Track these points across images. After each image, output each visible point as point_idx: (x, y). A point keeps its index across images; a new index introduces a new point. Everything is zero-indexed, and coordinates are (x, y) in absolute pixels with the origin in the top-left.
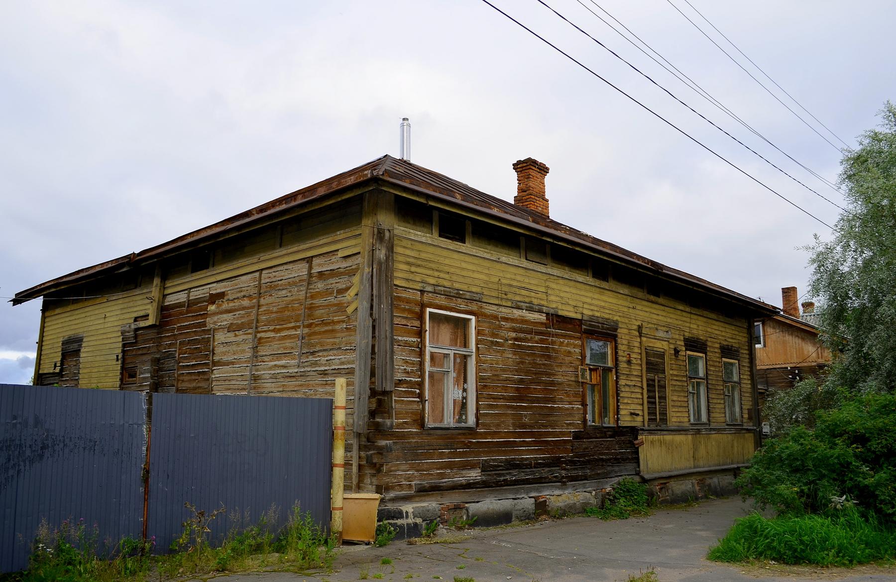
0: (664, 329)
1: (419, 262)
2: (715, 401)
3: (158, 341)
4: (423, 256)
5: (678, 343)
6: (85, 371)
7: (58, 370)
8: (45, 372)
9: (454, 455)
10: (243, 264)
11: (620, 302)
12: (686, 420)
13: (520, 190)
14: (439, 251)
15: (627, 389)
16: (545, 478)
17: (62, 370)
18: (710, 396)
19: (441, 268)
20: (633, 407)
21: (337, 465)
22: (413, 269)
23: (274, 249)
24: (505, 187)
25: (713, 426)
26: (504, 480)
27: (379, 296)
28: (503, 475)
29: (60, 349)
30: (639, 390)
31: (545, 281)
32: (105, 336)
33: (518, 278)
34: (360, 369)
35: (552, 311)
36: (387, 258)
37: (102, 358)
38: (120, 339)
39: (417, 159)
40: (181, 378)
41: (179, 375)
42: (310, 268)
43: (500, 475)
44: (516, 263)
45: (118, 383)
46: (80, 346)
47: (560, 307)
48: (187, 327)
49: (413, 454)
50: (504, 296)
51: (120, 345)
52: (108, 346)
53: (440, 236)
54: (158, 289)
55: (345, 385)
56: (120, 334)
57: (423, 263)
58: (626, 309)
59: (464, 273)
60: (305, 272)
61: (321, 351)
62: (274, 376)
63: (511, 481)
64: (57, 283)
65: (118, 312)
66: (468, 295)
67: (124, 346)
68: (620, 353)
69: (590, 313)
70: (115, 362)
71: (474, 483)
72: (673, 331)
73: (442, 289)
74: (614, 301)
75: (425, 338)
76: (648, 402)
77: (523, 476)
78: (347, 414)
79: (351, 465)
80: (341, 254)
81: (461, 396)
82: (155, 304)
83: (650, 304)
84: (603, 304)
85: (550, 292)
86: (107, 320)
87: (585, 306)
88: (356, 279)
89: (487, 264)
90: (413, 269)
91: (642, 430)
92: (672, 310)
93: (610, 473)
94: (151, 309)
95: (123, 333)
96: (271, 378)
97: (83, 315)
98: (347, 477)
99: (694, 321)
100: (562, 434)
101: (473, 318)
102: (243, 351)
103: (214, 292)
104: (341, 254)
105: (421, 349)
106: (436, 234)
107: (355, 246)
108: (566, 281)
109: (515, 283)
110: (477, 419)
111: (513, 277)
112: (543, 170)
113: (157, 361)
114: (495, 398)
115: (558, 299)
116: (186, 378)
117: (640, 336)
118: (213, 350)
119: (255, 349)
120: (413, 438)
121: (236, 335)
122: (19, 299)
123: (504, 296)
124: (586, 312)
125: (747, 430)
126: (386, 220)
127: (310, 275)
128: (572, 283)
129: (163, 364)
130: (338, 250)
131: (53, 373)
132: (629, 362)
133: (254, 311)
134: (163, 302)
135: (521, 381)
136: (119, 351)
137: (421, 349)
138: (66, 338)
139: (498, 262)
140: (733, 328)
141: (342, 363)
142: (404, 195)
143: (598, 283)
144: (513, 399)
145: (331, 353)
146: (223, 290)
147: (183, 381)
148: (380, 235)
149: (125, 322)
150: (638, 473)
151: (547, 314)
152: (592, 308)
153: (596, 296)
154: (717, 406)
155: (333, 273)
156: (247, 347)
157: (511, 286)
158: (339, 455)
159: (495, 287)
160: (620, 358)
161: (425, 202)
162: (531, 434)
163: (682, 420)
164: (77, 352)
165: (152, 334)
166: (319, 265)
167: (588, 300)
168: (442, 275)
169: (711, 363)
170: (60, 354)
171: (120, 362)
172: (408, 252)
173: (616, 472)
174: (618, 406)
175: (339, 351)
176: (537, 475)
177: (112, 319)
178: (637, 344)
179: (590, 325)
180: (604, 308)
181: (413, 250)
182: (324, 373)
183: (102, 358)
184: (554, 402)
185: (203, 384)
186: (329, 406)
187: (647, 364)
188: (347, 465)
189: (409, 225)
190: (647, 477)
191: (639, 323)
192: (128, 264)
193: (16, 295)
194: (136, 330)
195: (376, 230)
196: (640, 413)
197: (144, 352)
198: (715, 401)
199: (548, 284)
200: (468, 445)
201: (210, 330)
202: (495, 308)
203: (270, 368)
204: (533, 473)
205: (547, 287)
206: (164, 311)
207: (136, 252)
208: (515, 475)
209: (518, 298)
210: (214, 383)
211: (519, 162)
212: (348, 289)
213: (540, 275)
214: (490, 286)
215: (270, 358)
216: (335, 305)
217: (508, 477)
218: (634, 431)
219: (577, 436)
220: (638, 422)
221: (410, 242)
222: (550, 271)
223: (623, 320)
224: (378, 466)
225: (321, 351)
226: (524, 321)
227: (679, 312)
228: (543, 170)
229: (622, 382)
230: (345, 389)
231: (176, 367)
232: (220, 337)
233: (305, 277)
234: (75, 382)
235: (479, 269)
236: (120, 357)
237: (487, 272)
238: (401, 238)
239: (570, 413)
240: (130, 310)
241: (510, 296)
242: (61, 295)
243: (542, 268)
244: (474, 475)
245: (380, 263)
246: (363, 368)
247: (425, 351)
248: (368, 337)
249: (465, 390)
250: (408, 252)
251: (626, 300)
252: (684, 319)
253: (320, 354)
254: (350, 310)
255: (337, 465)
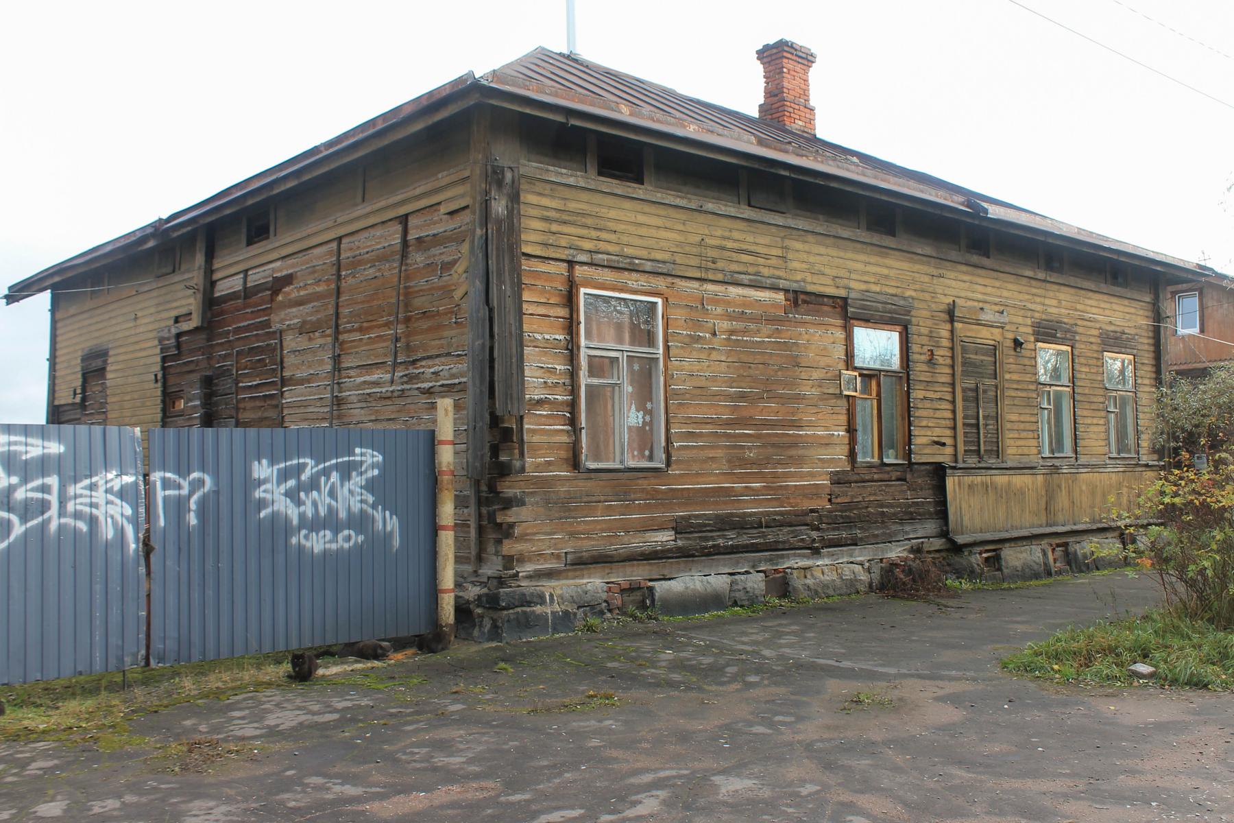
0: (997, 308)
1: (565, 217)
2: (1089, 421)
3: (208, 351)
4: (572, 206)
5: (1022, 329)
6: (114, 399)
7: (78, 399)
8: (62, 402)
9: (627, 510)
10: (315, 229)
11: (917, 267)
12: (1035, 451)
13: (769, 94)
14: (598, 198)
15: (928, 404)
16: (784, 542)
17: (84, 399)
18: (1078, 412)
19: (601, 223)
20: (938, 431)
21: (444, 528)
22: (555, 227)
23: (356, 205)
24: (745, 93)
25: (1083, 460)
26: (714, 546)
27: (499, 274)
28: (712, 538)
29: (79, 368)
30: (949, 406)
31: (783, 238)
32: (137, 347)
33: (736, 235)
34: (474, 384)
35: (795, 286)
36: (511, 212)
37: (135, 379)
38: (158, 351)
39: (595, 52)
40: (241, 405)
41: (238, 402)
42: (405, 232)
43: (706, 539)
44: (732, 211)
45: (160, 415)
46: (105, 362)
47: (809, 279)
48: (247, 328)
49: (564, 508)
50: (710, 265)
51: (158, 359)
52: (142, 362)
53: (600, 174)
54: (202, 272)
55: (451, 409)
56: (156, 342)
57: (371, 221)
58: (926, 279)
59: (643, 231)
60: (397, 240)
61: (423, 359)
62: (366, 398)
63: (726, 547)
64: (59, 269)
65: (152, 310)
66: (648, 266)
67: (164, 359)
68: (915, 348)
69: (863, 287)
70: (152, 385)
71: (662, 551)
72: (1012, 311)
73: (605, 257)
74: (905, 265)
75: (578, 334)
76: (964, 424)
77: (744, 540)
78: (456, 453)
79: (469, 526)
80: (443, 209)
81: (641, 421)
82: (200, 296)
83: (970, 269)
84: (885, 271)
85: (790, 256)
86: (139, 322)
87: (853, 276)
88: (465, 248)
89: (682, 215)
90: (555, 227)
91: (954, 468)
92: (1012, 278)
93: (895, 533)
94: (189, 302)
95: (161, 340)
96: (360, 401)
97: (106, 316)
98: (459, 543)
99: (1051, 294)
100: (812, 475)
101: (659, 301)
102: (321, 362)
103: (278, 275)
104: (443, 209)
105: (571, 351)
106: (592, 172)
107: (462, 196)
108: (820, 238)
109: (730, 245)
110: (669, 456)
111: (727, 234)
112: (806, 59)
113: (208, 382)
114: (697, 422)
115: (804, 266)
116: (249, 405)
117: (952, 321)
118: (282, 362)
119: (337, 359)
120: (563, 485)
121: (310, 339)
122: (18, 293)
123: (710, 265)
124: (853, 285)
125: (1147, 466)
126: (506, 154)
127: (405, 243)
128: (830, 241)
129: (217, 385)
130: (439, 203)
131: (73, 404)
132: (931, 362)
133: (332, 301)
134: (212, 292)
135: (742, 396)
136: (157, 368)
137: (571, 351)
138: (86, 352)
139: (699, 211)
140: (1126, 302)
141: (453, 376)
142: (528, 111)
143: (876, 238)
144: (729, 423)
145: (437, 361)
146: (290, 271)
147: (244, 409)
148: (495, 177)
149: (163, 324)
150: (944, 534)
151: (786, 291)
152: (866, 278)
153: (873, 259)
154: (1093, 429)
155: (437, 240)
156: (327, 356)
157: (723, 248)
158: (447, 511)
159: (694, 250)
160: (914, 357)
161: (563, 120)
162: (760, 476)
163: (1026, 451)
164: (101, 371)
165: (201, 339)
166: (417, 227)
167: (859, 266)
168: (604, 235)
169: (1082, 360)
170: (80, 376)
171: (159, 384)
172: (545, 202)
173: (907, 533)
174: (910, 431)
175: (449, 358)
176: (771, 538)
177: (146, 321)
178: (945, 333)
179: (864, 308)
180: (886, 277)
181: (553, 197)
182: (429, 392)
183: (135, 379)
184: (800, 427)
185: (272, 414)
186: (431, 441)
187: (964, 364)
188: (460, 527)
189: (547, 159)
190: (960, 540)
191: (950, 300)
192: (153, 235)
193: (10, 288)
194: (179, 335)
195: (489, 168)
196: (949, 441)
197: (192, 367)
198: (1089, 421)
199: (787, 242)
200: (654, 494)
201: (274, 332)
202: (696, 284)
203: (358, 387)
204: (764, 536)
205: (786, 248)
206: (213, 305)
207: (164, 217)
208: (732, 538)
209: (734, 267)
210: (285, 412)
211: (767, 48)
212: (454, 262)
213: (774, 229)
214: (687, 249)
215: (358, 371)
216: (440, 288)
217: (720, 541)
218: (939, 472)
219: (838, 480)
220: (944, 456)
221: (548, 186)
222: (791, 222)
223: (920, 295)
224: (504, 526)
225: (423, 359)
226: (747, 302)
227: (1024, 281)
228: (806, 59)
229: (917, 394)
230: (451, 414)
231: (234, 390)
232: (290, 342)
233: (398, 247)
234: (103, 416)
235: (669, 224)
236: (160, 376)
237: (681, 227)
238: (532, 180)
239: (827, 443)
240: (168, 306)
241: (720, 265)
242: (75, 285)
243: (779, 220)
244: (664, 538)
245: (499, 222)
246: (478, 382)
247: (578, 355)
248: (483, 336)
249: (650, 412)
250: (545, 202)
251: (928, 264)
252: (1034, 291)
253: (423, 363)
254: (458, 294)
255: (444, 528)
